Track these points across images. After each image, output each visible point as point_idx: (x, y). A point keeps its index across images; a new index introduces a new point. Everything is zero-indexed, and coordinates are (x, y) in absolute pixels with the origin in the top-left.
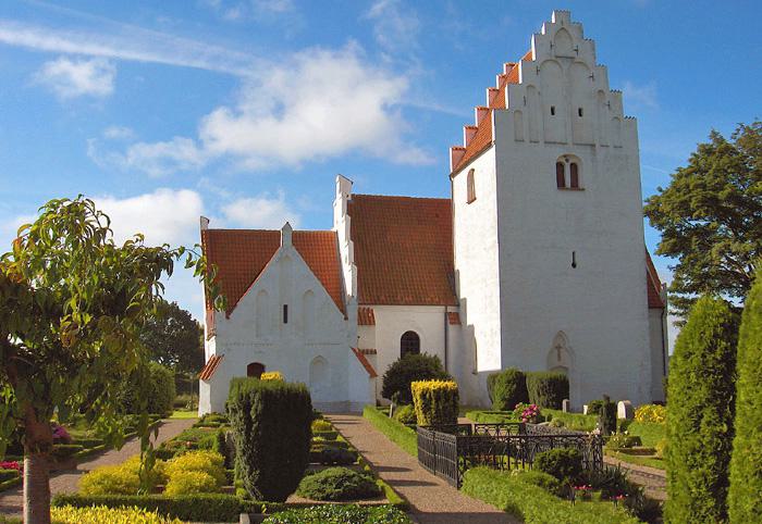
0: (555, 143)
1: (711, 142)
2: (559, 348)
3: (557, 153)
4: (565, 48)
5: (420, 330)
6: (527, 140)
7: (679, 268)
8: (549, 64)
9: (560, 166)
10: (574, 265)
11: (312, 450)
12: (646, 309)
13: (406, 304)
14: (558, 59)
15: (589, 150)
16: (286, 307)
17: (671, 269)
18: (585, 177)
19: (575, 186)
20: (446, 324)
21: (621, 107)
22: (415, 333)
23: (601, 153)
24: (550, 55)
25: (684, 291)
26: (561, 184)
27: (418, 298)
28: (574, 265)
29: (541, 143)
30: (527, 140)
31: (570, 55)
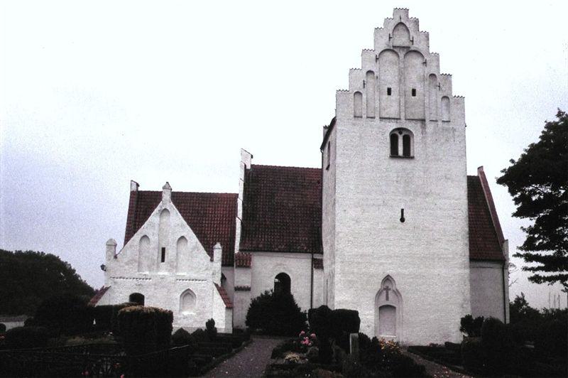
0: (389, 118)
1: (557, 120)
2: (387, 289)
3: (393, 126)
4: (401, 40)
5: (290, 271)
6: (364, 116)
7: (531, 231)
8: (388, 54)
9: (394, 138)
10: (402, 220)
11: (508, 322)
12: (466, 259)
13: (280, 251)
14: (392, 50)
15: (419, 124)
16: (163, 250)
17: (524, 230)
18: (416, 148)
19: (407, 155)
20: (312, 269)
21: (450, 88)
22: (289, 277)
23: (430, 127)
24: (388, 45)
25: (538, 248)
26: (394, 154)
27: (290, 248)
28: (402, 220)
29: (377, 118)
30: (364, 116)
31: (406, 45)
